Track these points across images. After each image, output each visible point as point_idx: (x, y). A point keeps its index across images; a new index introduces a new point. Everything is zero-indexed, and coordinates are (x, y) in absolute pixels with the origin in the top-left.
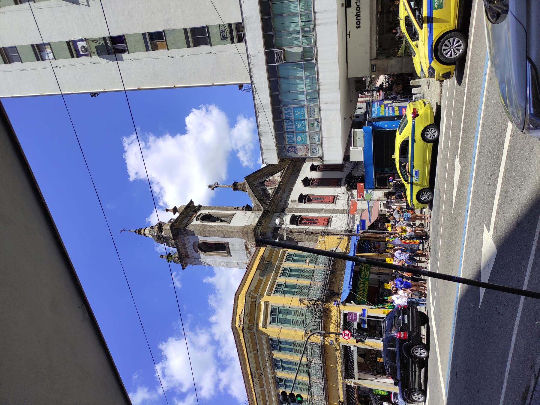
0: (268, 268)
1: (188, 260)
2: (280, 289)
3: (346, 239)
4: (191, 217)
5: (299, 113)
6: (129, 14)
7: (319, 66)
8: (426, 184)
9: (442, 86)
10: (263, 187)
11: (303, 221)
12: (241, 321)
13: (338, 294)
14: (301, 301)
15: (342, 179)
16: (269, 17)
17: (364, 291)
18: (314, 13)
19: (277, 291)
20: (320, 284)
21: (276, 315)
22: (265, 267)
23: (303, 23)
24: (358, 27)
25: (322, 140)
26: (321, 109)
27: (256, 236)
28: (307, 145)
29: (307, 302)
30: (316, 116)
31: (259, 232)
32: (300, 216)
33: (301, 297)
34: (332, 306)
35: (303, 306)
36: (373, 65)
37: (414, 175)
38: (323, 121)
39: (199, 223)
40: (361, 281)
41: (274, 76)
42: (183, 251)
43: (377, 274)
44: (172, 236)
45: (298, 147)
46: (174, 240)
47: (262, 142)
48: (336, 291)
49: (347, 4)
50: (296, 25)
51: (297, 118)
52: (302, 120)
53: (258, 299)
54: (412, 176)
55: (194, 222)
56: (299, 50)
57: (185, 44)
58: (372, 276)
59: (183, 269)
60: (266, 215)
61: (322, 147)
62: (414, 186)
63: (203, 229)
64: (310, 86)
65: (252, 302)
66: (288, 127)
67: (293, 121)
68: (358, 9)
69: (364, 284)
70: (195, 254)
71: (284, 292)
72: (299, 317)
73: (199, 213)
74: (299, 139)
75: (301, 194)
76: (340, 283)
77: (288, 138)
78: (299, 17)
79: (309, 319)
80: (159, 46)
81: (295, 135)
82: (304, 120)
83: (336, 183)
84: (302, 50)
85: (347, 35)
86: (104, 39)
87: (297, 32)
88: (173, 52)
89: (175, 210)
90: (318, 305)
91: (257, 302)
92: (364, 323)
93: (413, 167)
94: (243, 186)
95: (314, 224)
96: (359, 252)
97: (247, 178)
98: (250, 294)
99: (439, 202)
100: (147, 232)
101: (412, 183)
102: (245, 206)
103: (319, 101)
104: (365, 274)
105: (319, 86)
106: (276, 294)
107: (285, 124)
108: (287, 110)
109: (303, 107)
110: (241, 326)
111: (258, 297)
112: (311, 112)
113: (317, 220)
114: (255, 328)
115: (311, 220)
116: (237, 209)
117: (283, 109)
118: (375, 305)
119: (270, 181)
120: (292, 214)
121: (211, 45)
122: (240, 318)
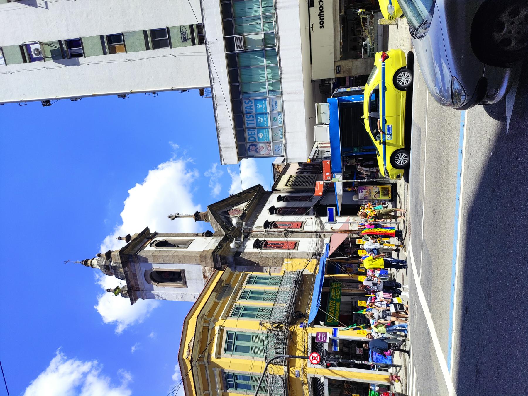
1: (138, 293)
2: (238, 312)
3: (314, 261)
4: (145, 244)
5: (260, 106)
6: (87, 16)
7: (281, 52)
8: (401, 144)
10: (226, 216)
12: (190, 351)
13: (305, 316)
14: (261, 324)
19: (234, 315)
20: (285, 305)
21: (233, 343)
22: (222, 290)
23: (264, 9)
24: (322, 27)
25: (285, 136)
27: (215, 261)
28: (269, 143)
29: (269, 325)
30: (279, 109)
31: (219, 255)
32: (265, 240)
33: (262, 320)
34: (298, 329)
35: (265, 330)
36: (338, 67)
37: (386, 132)
39: (153, 249)
40: (331, 302)
42: (133, 282)
43: (349, 295)
44: (121, 265)
45: (261, 145)
47: (220, 139)
48: (303, 312)
49: (311, 4)
51: (258, 112)
52: (263, 114)
53: (211, 323)
54: (384, 134)
55: (148, 248)
56: (261, 37)
58: (344, 299)
59: (132, 304)
60: (227, 239)
62: (386, 146)
66: (249, 122)
67: (255, 116)
68: (321, 9)
69: (335, 306)
70: (147, 286)
71: (243, 315)
73: (154, 240)
74: (261, 135)
75: (267, 221)
78: (260, 3)
80: (117, 49)
81: (256, 131)
82: (266, 114)
83: (303, 211)
84: (263, 37)
85: (311, 28)
86: (60, 42)
87: (258, 18)
88: (131, 55)
90: (281, 328)
91: (210, 327)
92: (336, 346)
93: (385, 122)
94: (206, 215)
95: (281, 248)
96: (329, 273)
97: (210, 207)
98: (202, 317)
100: (94, 262)
101: (384, 143)
102: (205, 232)
103: (282, 92)
104: (336, 296)
105: (281, 74)
106: (233, 317)
107: (246, 119)
108: (248, 103)
109: (265, 100)
110: (190, 357)
111: (211, 321)
112: (273, 106)
113: (283, 244)
114: (206, 359)
115: (278, 244)
116: (197, 235)
117: (243, 101)
118: (348, 326)
119: (234, 210)
120: (255, 239)
121: (171, 48)
122: (189, 348)
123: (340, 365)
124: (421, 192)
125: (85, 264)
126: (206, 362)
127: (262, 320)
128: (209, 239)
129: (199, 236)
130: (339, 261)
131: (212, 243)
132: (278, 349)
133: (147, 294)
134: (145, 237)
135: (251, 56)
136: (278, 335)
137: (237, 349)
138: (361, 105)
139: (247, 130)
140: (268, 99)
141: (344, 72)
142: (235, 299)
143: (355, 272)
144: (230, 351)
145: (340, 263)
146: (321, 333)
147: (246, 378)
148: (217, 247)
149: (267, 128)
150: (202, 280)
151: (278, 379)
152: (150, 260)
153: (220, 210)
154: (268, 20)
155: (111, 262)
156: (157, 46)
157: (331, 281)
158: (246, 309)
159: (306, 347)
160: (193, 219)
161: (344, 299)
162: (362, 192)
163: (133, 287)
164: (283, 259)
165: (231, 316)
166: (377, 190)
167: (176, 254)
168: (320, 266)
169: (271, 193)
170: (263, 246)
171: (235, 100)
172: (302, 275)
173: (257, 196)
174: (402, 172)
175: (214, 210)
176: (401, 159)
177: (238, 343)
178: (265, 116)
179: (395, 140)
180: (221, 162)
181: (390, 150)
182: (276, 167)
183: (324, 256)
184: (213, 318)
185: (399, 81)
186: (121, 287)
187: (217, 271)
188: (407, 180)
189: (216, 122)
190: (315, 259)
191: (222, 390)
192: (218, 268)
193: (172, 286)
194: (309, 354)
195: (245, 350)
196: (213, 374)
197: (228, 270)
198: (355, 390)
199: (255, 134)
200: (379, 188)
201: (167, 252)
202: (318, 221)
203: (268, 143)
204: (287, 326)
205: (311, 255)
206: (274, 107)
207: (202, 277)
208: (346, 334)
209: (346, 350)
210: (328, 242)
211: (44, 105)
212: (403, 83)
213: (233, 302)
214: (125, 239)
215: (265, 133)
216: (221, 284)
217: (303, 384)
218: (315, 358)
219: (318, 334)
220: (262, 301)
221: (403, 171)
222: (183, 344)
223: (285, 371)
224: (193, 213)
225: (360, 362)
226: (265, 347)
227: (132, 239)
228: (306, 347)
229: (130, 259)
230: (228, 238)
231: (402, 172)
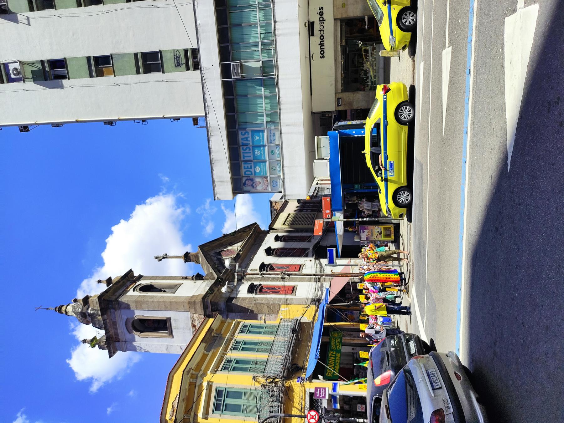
0: (217, 342)
3: (313, 307)
4: (128, 288)
5: (257, 138)
6: (73, 35)
7: (280, 81)
8: (403, 181)
9: (414, 61)
10: (219, 257)
12: (173, 411)
15: (309, 249)
16: (225, 26)
17: (335, 365)
18: (275, 22)
19: (225, 368)
20: (281, 357)
22: (212, 340)
23: (263, 35)
25: (283, 170)
26: (282, 132)
27: (205, 308)
29: (263, 380)
31: (209, 301)
32: (260, 285)
34: (295, 384)
35: (258, 385)
36: (338, 99)
37: (388, 169)
39: (137, 293)
41: (229, 90)
42: (112, 332)
44: (100, 312)
45: (258, 180)
46: (102, 315)
47: (214, 172)
48: (300, 365)
50: (256, 36)
51: (255, 144)
52: (260, 146)
53: (199, 379)
55: (131, 293)
56: (259, 65)
57: (134, 70)
58: (345, 349)
59: (110, 357)
60: (219, 283)
64: (271, 106)
65: (191, 383)
66: (246, 155)
68: (322, 38)
69: (336, 357)
70: (128, 336)
71: (234, 369)
72: (251, 401)
73: (138, 283)
74: (258, 169)
75: (263, 263)
76: (306, 357)
79: (265, 401)
80: (105, 72)
81: (252, 165)
82: (264, 146)
83: (302, 253)
84: (261, 65)
85: (311, 57)
86: (42, 62)
87: (256, 45)
88: (120, 79)
89: (109, 281)
90: (276, 383)
91: (198, 383)
92: (335, 402)
93: (386, 158)
95: (277, 293)
96: (328, 320)
97: (202, 247)
98: (189, 372)
99: (422, 177)
100: (70, 309)
101: (386, 180)
102: (195, 275)
103: (280, 123)
104: (336, 346)
105: (279, 104)
106: (223, 371)
107: (242, 151)
108: (244, 135)
109: (263, 131)
110: (173, 418)
111: (199, 375)
112: (271, 139)
115: (274, 288)
116: (186, 278)
117: (240, 133)
118: (349, 380)
119: (228, 250)
120: (250, 283)
121: (163, 72)
122: (173, 407)
124: (424, 232)
125: (59, 311)
127: (255, 374)
129: (189, 279)
132: (272, 407)
133: (128, 346)
134: (128, 280)
135: (249, 84)
136: (272, 391)
137: (229, 408)
138: (362, 139)
139: (243, 163)
140: (265, 130)
143: (357, 319)
144: (219, 410)
145: (340, 310)
146: (320, 388)
148: (208, 292)
149: (265, 162)
150: (190, 329)
152: (133, 307)
153: (212, 250)
154: (267, 47)
155: (88, 308)
156: (148, 70)
157: (331, 330)
158: (237, 362)
160: (182, 260)
161: (345, 349)
162: (364, 232)
163: (112, 338)
164: (279, 305)
165: (221, 370)
166: (379, 230)
167: (162, 300)
168: (319, 313)
169: (268, 232)
170: (258, 291)
171: (231, 130)
172: (300, 323)
174: (404, 211)
175: (206, 250)
176: (403, 198)
177: (229, 401)
178: (262, 148)
179: (397, 177)
180: (214, 197)
181: (392, 188)
182: (274, 204)
183: (323, 302)
185: (401, 115)
186: (98, 338)
187: (207, 318)
188: (410, 220)
189: (210, 153)
190: (314, 306)
192: (208, 316)
193: (156, 337)
194: (306, 412)
195: (236, 409)
197: (219, 317)
199: (251, 168)
200: (381, 228)
201: (152, 297)
202: (318, 263)
203: (265, 177)
204: (283, 380)
207: (191, 325)
209: (346, 407)
210: (328, 287)
211: (21, 131)
212: (405, 118)
214: (105, 282)
215: (262, 167)
216: (211, 333)
219: (316, 389)
222: (166, 403)
224: (182, 254)
226: (258, 405)
227: (114, 282)
228: (303, 404)
229: (110, 306)
230: (221, 282)
231: (404, 211)
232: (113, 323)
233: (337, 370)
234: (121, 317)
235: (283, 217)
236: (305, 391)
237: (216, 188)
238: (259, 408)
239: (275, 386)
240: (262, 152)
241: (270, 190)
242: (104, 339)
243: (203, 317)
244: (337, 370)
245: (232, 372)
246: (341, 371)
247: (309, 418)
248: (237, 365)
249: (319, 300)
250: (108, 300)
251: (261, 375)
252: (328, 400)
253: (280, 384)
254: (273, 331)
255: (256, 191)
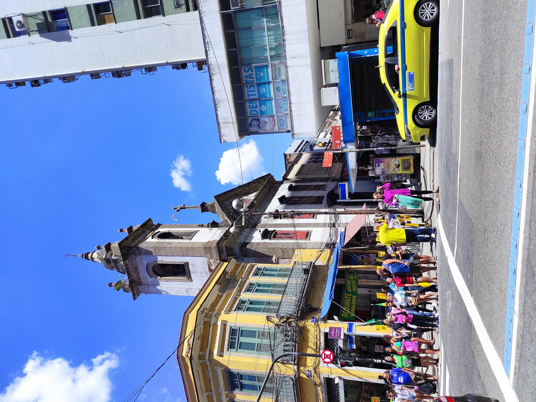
1: (140, 287)
2: (241, 306)
3: (328, 251)
4: (147, 235)
8: (426, 97)
11: (277, 236)
12: (189, 348)
13: (317, 310)
14: (268, 319)
15: (323, 197)
17: (351, 307)
19: (239, 308)
20: (294, 298)
21: (236, 339)
22: (227, 282)
25: (290, 107)
27: (220, 252)
28: (273, 116)
29: (276, 320)
32: (274, 231)
33: (269, 314)
34: (309, 324)
36: (349, 30)
38: (291, 81)
39: (155, 240)
42: (134, 276)
47: (219, 113)
48: (315, 305)
52: (265, 83)
55: (150, 240)
58: (361, 291)
59: (135, 299)
61: (291, 116)
63: (158, 246)
65: (205, 323)
66: (250, 93)
69: (352, 299)
70: (150, 280)
71: (248, 309)
72: (264, 340)
73: (156, 231)
77: (250, 108)
82: (269, 83)
86: (44, 13)
88: (121, 26)
91: (212, 323)
92: (351, 342)
93: (405, 68)
94: (213, 206)
95: (291, 238)
96: (344, 263)
98: (203, 312)
100: (95, 255)
101: (404, 96)
103: (285, 56)
104: (352, 288)
105: (283, 35)
107: (246, 88)
109: (267, 66)
110: (189, 355)
111: (213, 315)
114: (207, 357)
115: (288, 234)
116: (202, 226)
117: (243, 70)
118: (366, 321)
122: (189, 345)
123: (357, 364)
124: (454, 143)
125: (85, 257)
126: (207, 360)
127: (269, 314)
128: (215, 230)
130: (355, 251)
131: (216, 234)
132: (287, 346)
134: (147, 229)
136: (286, 331)
137: (242, 346)
138: (375, 60)
139: (247, 103)
140: (270, 65)
141: (356, 37)
142: (240, 292)
143: (373, 262)
144: (234, 348)
145: (356, 254)
146: (335, 328)
147: (252, 378)
148: (222, 237)
149: (270, 100)
151: (287, 379)
155: (112, 254)
157: (346, 272)
158: (251, 303)
159: (318, 344)
161: (361, 291)
162: (379, 166)
163: (135, 281)
164: (294, 250)
166: (397, 163)
167: (179, 246)
168: (334, 257)
169: (281, 183)
170: (272, 236)
172: (314, 266)
173: (266, 186)
174: (426, 132)
175: (221, 200)
176: (426, 115)
177: (243, 339)
179: (418, 91)
180: (220, 140)
181: (412, 105)
182: (288, 157)
184: (215, 312)
185: (422, 14)
186: (122, 281)
187: (222, 262)
188: (433, 143)
189: (213, 93)
190: (329, 250)
191: (226, 391)
194: (321, 351)
195: (250, 347)
196: (215, 373)
197: (233, 261)
198: (376, 392)
199: (256, 107)
200: (398, 160)
201: (170, 243)
204: (297, 320)
205: (324, 246)
206: (278, 75)
207: (207, 269)
208: (363, 329)
209: (364, 348)
210: (343, 230)
211: (33, 86)
212: (427, 18)
213: (237, 295)
215: (268, 105)
216: (225, 276)
217: (316, 384)
218: (327, 357)
219: (331, 329)
220: (268, 294)
221: (428, 130)
223: (294, 370)
225: (380, 361)
226: (272, 344)
228: (318, 344)
229: (131, 252)
231: (426, 132)
232: (135, 268)
233: (353, 311)
234: (142, 262)
235: (296, 168)
236: (320, 331)
237: (222, 130)
238: (272, 346)
239: (289, 326)
240: (268, 90)
241: (277, 130)
242: (127, 283)
243: (219, 261)
244: (353, 311)
245: (245, 312)
246: (357, 312)
247: (323, 358)
248: (251, 306)
249: (334, 244)
250: (129, 247)
251: (275, 315)
252: (344, 340)
253: (294, 324)
254: (288, 273)
255: (262, 131)
